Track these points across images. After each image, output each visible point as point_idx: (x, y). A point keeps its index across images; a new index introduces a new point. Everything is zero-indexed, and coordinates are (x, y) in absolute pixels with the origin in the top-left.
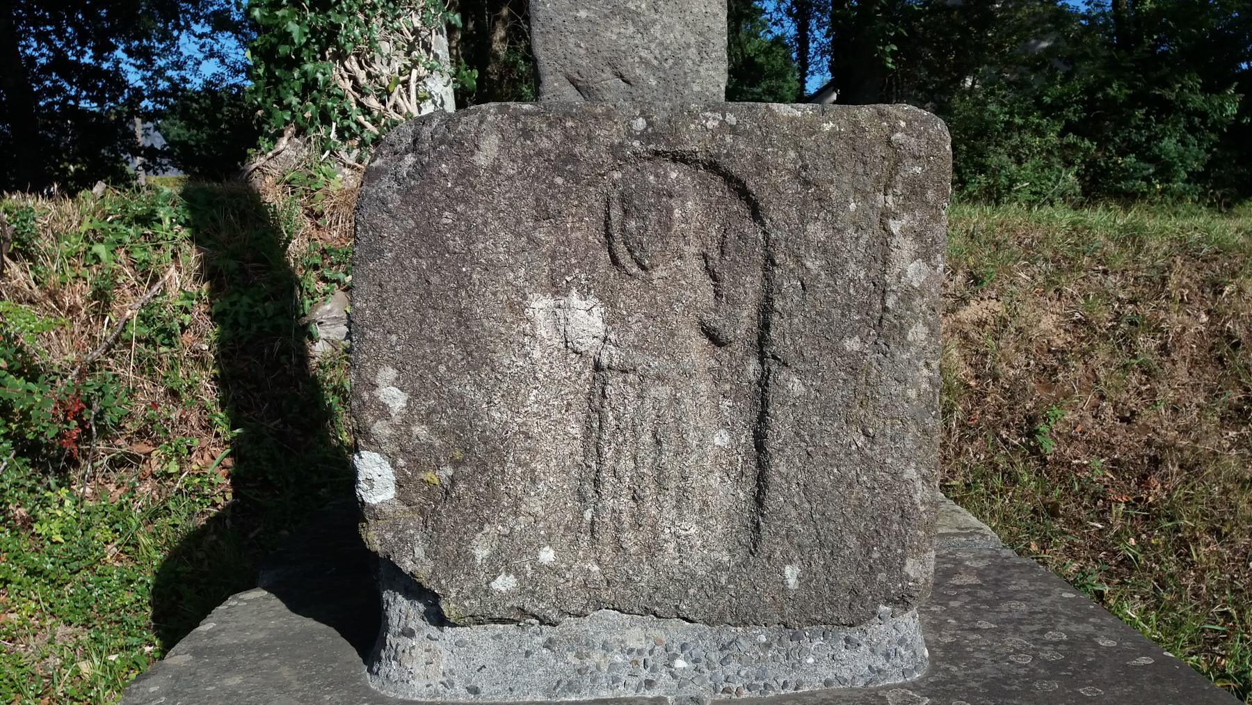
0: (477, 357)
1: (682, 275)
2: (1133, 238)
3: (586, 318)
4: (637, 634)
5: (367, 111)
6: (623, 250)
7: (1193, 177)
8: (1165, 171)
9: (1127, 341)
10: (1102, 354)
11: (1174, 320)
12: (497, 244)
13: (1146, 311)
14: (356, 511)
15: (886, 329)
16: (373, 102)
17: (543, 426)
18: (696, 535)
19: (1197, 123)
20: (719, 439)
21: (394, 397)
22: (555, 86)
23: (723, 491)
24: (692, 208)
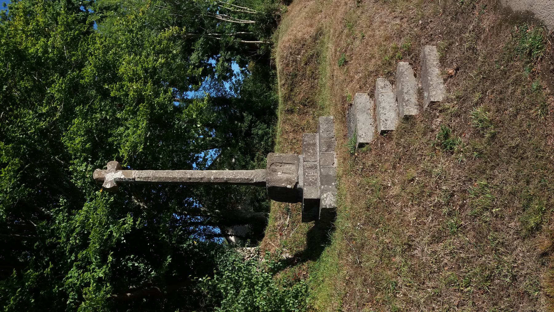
0: (281, 179)
1: (276, 168)
2: (280, 143)
3: (279, 173)
4: (299, 171)
5: (253, 256)
6: (275, 171)
7: (268, 127)
8: (266, 133)
9: (294, 143)
10: (295, 147)
11: (291, 137)
12: (275, 178)
13: (289, 141)
14: (291, 188)
15: (281, 156)
16: (252, 255)
17: (285, 176)
18: (293, 167)
19: (252, 124)
20: (287, 166)
21: (284, 184)
22: (265, 180)
23: (291, 166)
24: (273, 167)
